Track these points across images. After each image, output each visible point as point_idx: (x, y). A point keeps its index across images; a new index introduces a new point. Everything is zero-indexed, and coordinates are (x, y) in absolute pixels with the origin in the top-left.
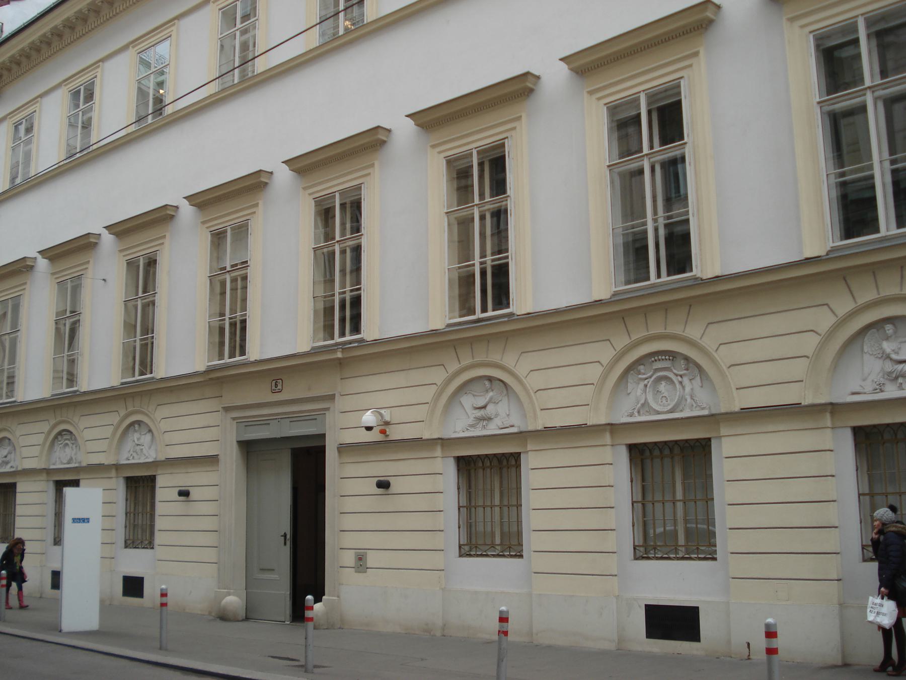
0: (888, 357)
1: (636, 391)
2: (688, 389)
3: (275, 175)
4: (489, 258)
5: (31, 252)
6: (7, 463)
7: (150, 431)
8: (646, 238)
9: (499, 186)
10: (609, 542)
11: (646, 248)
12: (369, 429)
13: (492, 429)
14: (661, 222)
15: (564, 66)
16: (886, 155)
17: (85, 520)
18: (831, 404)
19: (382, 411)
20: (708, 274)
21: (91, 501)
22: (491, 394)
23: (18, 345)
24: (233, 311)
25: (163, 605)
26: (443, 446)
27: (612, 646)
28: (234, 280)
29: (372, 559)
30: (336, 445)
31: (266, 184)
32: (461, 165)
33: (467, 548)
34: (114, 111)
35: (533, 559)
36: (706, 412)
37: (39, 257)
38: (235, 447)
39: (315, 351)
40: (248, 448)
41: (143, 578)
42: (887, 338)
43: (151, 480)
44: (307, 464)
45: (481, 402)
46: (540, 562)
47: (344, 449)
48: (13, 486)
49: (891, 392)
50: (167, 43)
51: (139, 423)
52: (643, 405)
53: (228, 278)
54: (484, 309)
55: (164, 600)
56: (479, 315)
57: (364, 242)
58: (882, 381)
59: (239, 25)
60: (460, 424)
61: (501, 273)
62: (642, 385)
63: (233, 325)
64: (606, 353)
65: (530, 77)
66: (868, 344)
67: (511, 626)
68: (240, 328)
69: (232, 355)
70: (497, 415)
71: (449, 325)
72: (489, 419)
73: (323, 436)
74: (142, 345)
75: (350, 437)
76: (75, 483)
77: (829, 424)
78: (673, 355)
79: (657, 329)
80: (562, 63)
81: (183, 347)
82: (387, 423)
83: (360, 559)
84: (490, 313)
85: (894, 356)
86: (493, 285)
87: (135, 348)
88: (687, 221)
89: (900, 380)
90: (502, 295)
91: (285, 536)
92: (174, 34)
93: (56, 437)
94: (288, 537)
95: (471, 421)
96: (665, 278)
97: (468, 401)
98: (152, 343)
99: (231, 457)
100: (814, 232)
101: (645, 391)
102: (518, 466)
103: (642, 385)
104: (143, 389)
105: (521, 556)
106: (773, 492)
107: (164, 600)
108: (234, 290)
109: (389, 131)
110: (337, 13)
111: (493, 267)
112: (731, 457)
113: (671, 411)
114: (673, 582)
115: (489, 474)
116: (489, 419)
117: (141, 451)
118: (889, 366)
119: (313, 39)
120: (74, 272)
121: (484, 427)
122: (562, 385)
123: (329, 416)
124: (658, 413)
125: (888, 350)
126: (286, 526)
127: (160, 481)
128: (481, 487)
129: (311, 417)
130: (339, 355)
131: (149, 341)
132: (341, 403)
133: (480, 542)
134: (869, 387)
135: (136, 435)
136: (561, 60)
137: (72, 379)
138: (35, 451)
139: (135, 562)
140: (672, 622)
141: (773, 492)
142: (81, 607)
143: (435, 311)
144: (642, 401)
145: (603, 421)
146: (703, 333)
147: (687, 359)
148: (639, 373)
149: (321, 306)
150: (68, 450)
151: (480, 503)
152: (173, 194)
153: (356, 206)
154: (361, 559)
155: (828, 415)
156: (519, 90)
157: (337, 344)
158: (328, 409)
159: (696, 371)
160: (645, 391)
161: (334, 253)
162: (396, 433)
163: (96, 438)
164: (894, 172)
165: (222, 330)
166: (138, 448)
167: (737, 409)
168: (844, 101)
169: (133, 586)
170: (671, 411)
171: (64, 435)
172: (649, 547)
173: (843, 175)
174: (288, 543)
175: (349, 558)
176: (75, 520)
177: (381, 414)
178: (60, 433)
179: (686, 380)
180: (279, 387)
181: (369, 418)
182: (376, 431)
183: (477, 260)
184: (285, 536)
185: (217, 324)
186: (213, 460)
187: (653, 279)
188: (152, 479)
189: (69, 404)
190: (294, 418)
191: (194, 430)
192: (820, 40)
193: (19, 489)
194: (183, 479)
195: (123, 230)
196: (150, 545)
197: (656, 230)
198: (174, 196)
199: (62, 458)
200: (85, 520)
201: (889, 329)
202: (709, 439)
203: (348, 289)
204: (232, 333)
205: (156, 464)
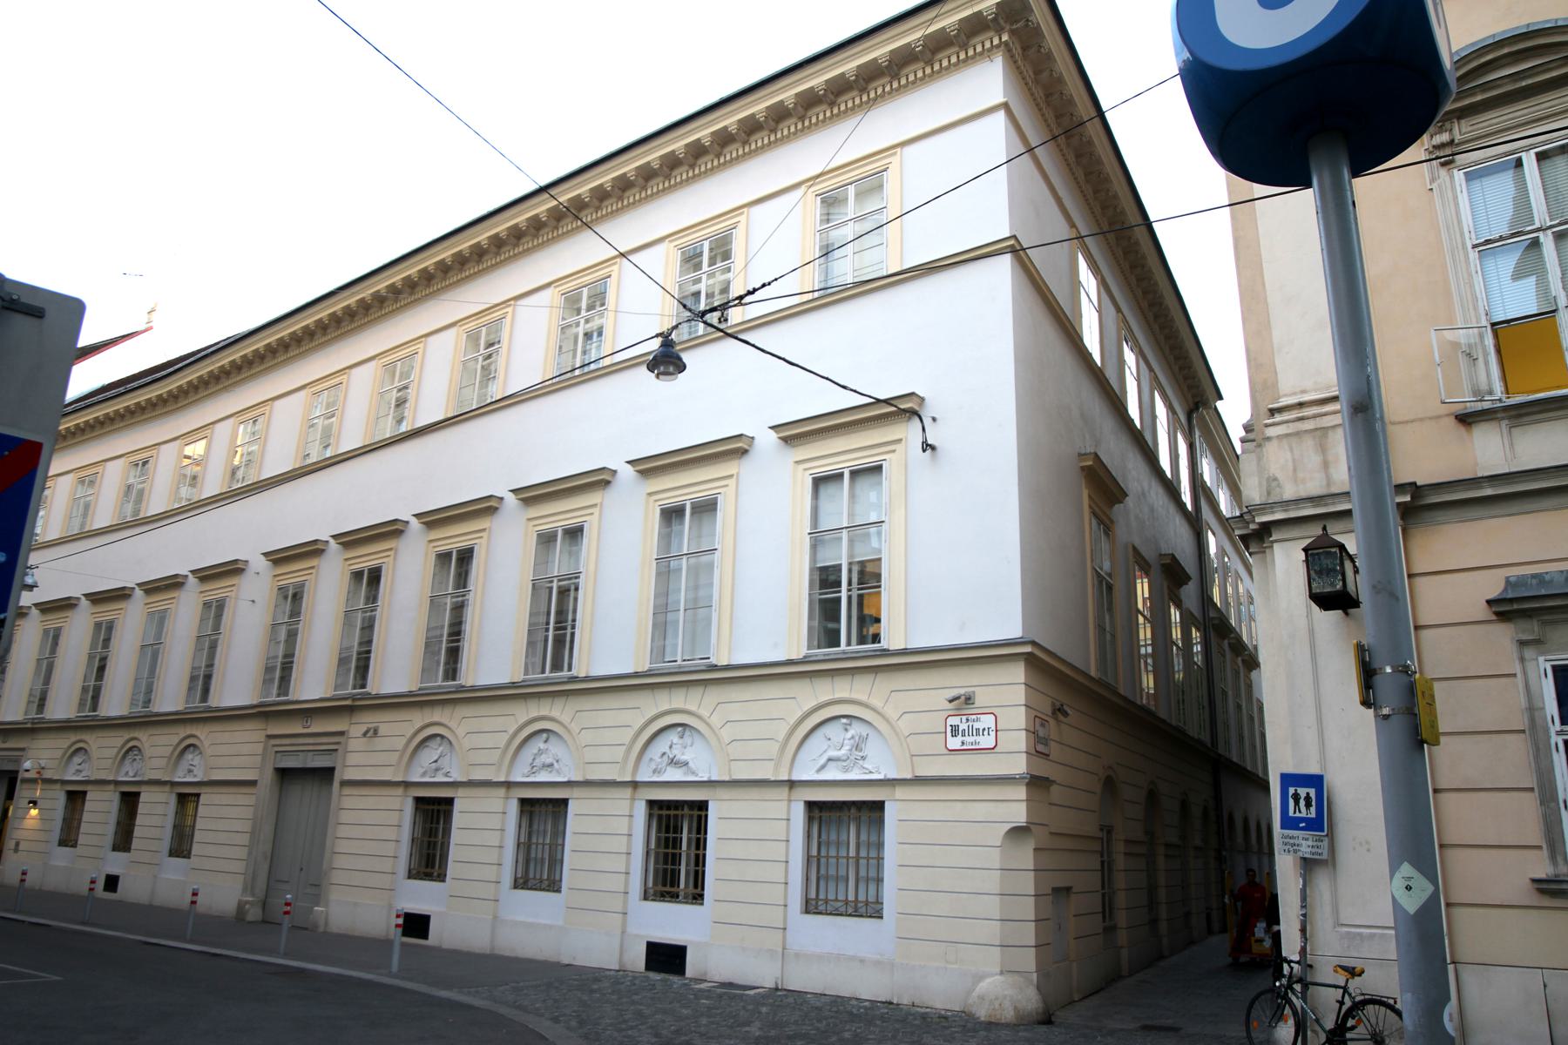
3: (756, 442)
5: (183, 570)
11: (564, 642)
14: (855, 593)
23: (219, 649)
34: (529, 349)
39: (804, 661)
40: (284, 774)
43: (83, 795)
48: (450, 802)
59: (583, 313)
64: (119, 742)
67: (28, 877)
74: (555, 637)
98: (573, 634)
99: (267, 778)
115: (844, 824)
117: (194, 770)
120: (219, 595)
133: (831, 896)
136: (265, 554)
137: (148, 702)
145: (502, 779)
152: (251, 552)
154: (17, 844)
156: (734, 449)
162: (47, 775)
171: (131, 751)
178: (131, 749)
186: (253, 783)
187: (843, 646)
191: (238, 753)
193: (89, 797)
195: (351, 540)
199: (128, 773)
204: (282, 669)
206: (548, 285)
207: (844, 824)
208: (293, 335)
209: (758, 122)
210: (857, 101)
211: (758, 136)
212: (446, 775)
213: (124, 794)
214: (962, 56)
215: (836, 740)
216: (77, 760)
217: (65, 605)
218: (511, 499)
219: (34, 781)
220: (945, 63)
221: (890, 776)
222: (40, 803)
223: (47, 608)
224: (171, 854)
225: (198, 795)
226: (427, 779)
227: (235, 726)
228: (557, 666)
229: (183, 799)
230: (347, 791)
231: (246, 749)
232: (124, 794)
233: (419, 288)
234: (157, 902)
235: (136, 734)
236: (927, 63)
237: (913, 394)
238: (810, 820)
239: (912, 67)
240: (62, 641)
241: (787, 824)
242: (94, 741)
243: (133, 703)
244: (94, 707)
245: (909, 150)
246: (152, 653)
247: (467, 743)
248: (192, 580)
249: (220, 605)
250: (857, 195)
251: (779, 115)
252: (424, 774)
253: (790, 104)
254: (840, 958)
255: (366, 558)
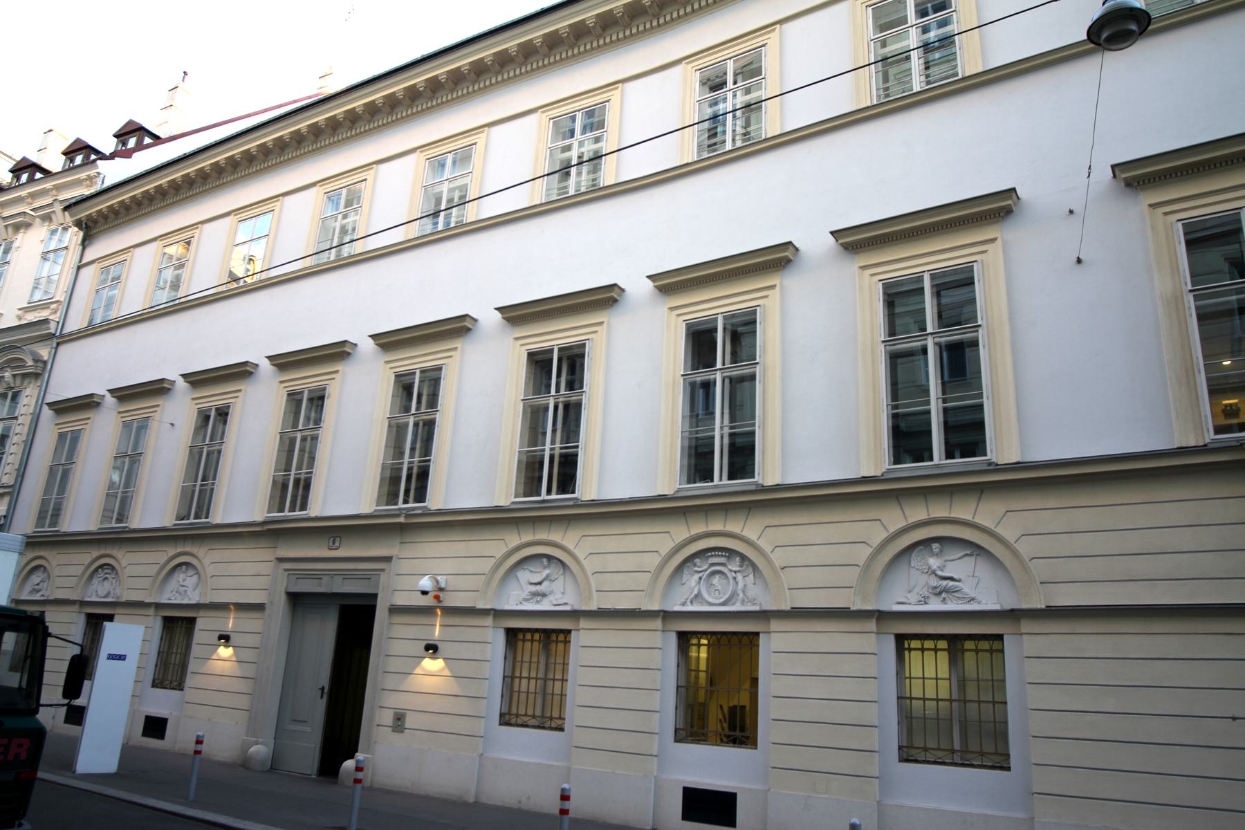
0: (934, 572)
1: (691, 581)
2: (741, 585)
4: (558, 445)
6: (38, 591)
7: (198, 573)
8: (713, 445)
9: (433, 402)
10: (871, 740)
12: (424, 593)
13: (545, 606)
14: (727, 431)
15: (498, 315)
16: (726, 422)
17: (121, 658)
18: (879, 611)
19: (439, 578)
20: (769, 481)
21: (129, 639)
22: (547, 571)
23: (71, 476)
24: (299, 467)
25: (197, 752)
26: (878, 620)
27: (472, 800)
28: (304, 439)
29: (410, 721)
30: (388, 605)
31: (349, 354)
32: (407, 380)
33: (683, 733)
35: (189, 694)
36: (757, 608)
37: (108, 395)
38: (283, 597)
40: (297, 600)
41: (735, 795)
42: (933, 555)
44: (356, 621)
45: (537, 579)
46: (582, 738)
47: (395, 610)
49: (935, 605)
50: (270, 216)
51: (187, 564)
52: (696, 596)
53: (299, 435)
54: (549, 492)
55: (199, 747)
56: (544, 496)
57: (438, 416)
58: (927, 594)
60: (515, 598)
61: (424, 475)
62: (696, 577)
63: (297, 481)
65: (791, 248)
66: (916, 560)
68: (304, 486)
69: (292, 509)
70: (552, 592)
71: (513, 503)
72: (544, 595)
73: (375, 596)
75: (401, 600)
76: (110, 618)
77: (660, 627)
78: (730, 553)
79: (717, 526)
80: (370, 340)
81: (243, 496)
82: (441, 590)
83: (399, 719)
84: (554, 496)
85: (939, 573)
86: (559, 474)
87: (193, 492)
88: (753, 433)
89: (944, 595)
90: (567, 480)
91: (323, 689)
92: (277, 209)
93: (96, 570)
94: (326, 690)
95: (525, 595)
96: (725, 482)
97: (525, 576)
99: (280, 605)
100: (869, 455)
101: (699, 583)
102: (567, 642)
103: (696, 577)
104: (195, 530)
105: (1009, 769)
106: (816, 689)
107: (199, 747)
108: (302, 450)
109: (476, 320)
110: (580, 164)
111: (561, 456)
112: (587, 645)
113: (723, 604)
114: (713, 766)
115: (537, 644)
116: (544, 595)
117: (184, 591)
118: (934, 582)
119: (536, 194)
120: (315, 383)
121: (538, 602)
122: (616, 567)
123: (383, 576)
124: (711, 604)
125: (934, 567)
126: (324, 679)
127: (200, 624)
128: (526, 658)
129: (366, 577)
130: (402, 520)
131: (209, 488)
132: (397, 566)
133: (522, 711)
134: (913, 598)
135: (182, 576)
136: (832, 233)
138: (146, 583)
139: (161, 703)
140: (708, 805)
141: (816, 689)
142: (100, 747)
143: (662, 474)
144: (696, 592)
145: (657, 608)
146: (576, 542)
147: (743, 558)
148: (695, 565)
149: (388, 474)
150: (106, 584)
151: (525, 674)
153: (435, 383)
155: (874, 621)
157: (400, 509)
158: (383, 570)
159: (750, 570)
160: (699, 583)
161: (407, 425)
162: (451, 600)
163: (137, 573)
164: (895, 417)
165: (285, 487)
166: (182, 589)
167: (788, 608)
168: (540, 400)
169: (155, 727)
170: (723, 604)
172: (693, 728)
173: (697, 432)
174: (325, 697)
175: (387, 718)
176: (112, 657)
177: (437, 582)
178: (101, 566)
179: (739, 577)
180: (337, 544)
181: (426, 583)
182: (431, 595)
183: (548, 446)
184: (323, 689)
185: (280, 480)
186: (260, 607)
188: (191, 621)
189: (117, 537)
190: (347, 576)
191: (248, 574)
192: (690, 327)
194: (230, 623)
196: (180, 687)
197: (722, 437)
198: (257, 355)
199: (99, 591)
200: (121, 658)
201: (935, 546)
202: (757, 634)
203: (417, 459)
204: (293, 486)
205: (198, 607)
206: (313, 185)
207: (537, 644)
208: (159, 189)
209: (462, 73)
210: (595, 44)
211: (639, 21)
212: (753, 602)
213: (90, 616)
214: (655, 23)
215: (186, 580)
216: (36, 579)
217: (87, 403)
218: (181, 383)
219: (427, 611)
220: (641, 28)
221: (577, 607)
222: (234, 639)
223: (63, 408)
224: (154, 685)
225: (568, 632)
226: (690, 608)
227: (615, 528)
228: (119, 520)
229: (170, 623)
230: (398, 619)
231: (251, 569)
232: (90, 616)
233: (209, 180)
234: (484, 800)
235: (42, 553)
236: (654, 15)
237: (615, 285)
238: (164, 627)
239: (644, 20)
240: (82, 445)
241: (657, 655)
242: (125, 558)
243: (106, 516)
244: (54, 523)
245: (629, 86)
246: (129, 459)
247: (130, 571)
248: (110, 400)
249: (76, 437)
250: (454, 162)
251: (413, 95)
252: (684, 604)
253: (538, 42)
254: (522, 765)
255: (213, 397)
